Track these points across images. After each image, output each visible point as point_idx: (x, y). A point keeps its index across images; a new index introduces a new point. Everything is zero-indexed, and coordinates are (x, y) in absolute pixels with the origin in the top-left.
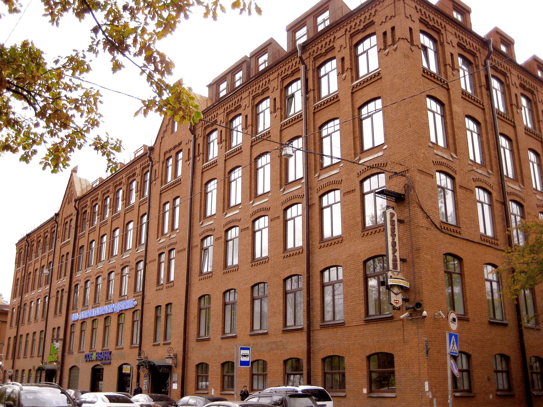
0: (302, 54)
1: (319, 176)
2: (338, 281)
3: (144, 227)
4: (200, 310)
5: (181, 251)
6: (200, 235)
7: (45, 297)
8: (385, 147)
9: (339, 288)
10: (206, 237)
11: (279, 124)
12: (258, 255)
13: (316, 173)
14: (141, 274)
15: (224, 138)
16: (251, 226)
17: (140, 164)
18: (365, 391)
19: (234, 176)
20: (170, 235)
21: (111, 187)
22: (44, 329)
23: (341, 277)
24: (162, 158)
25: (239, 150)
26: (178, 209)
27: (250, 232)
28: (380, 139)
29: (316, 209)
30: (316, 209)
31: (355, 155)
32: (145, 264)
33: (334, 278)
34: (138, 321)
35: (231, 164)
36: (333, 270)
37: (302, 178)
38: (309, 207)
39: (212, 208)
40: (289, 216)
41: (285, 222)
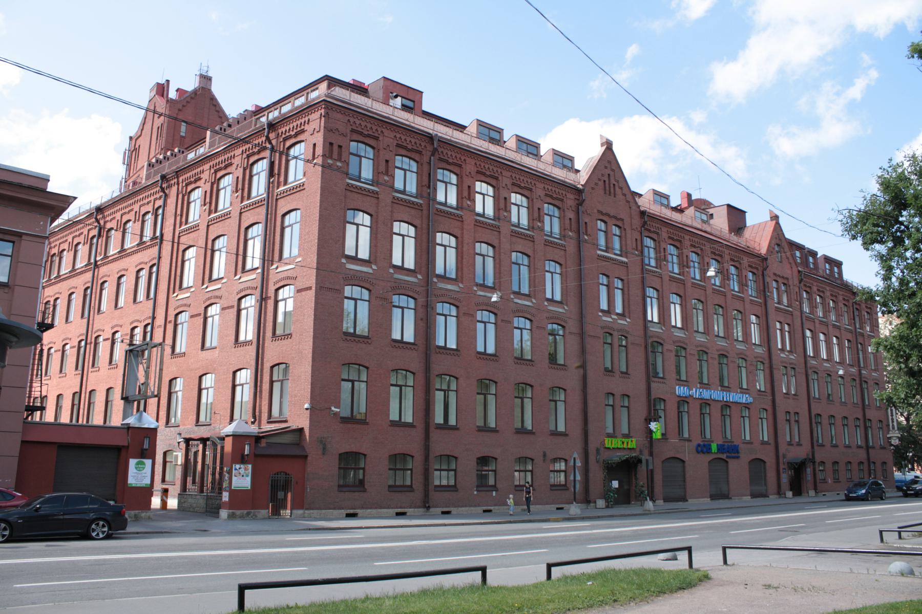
0: (268, 133)
1: (277, 268)
4: (272, 382)
5: (228, 308)
6: (275, 283)
7: (146, 326)
9: (211, 390)
10: (211, 305)
11: (238, 206)
13: (174, 292)
14: (82, 350)
16: (203, 312)
17: (241, 149)
19: (219, 244)
20: (277, 268)
21: (207, 173)
22: (78, 390)
25: (227, 216)
29: (271, 303)
30: (271, 303)
32: (86, 344)
35: (214, 231)
37: (257, 268)
38: (263, 299)
40: (280, 297)
41: (205, 319)
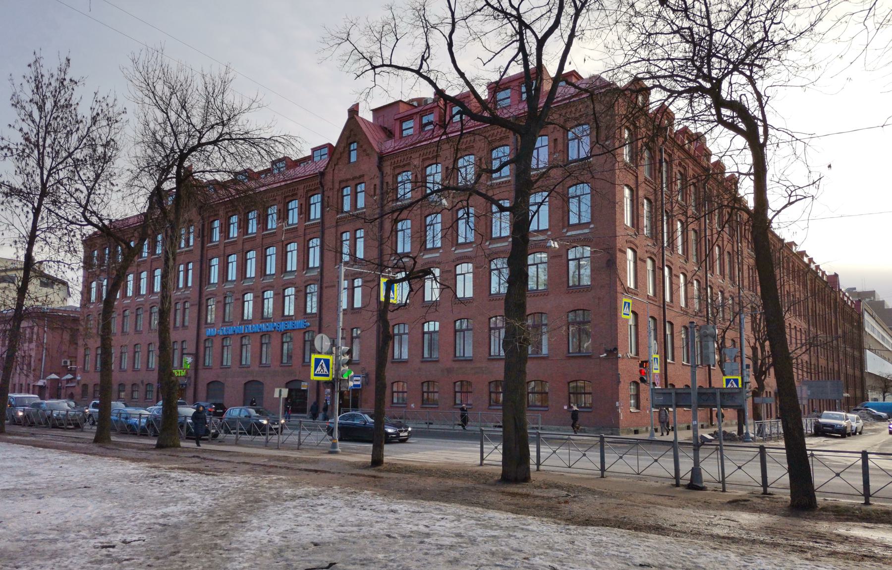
2: (435, 332)
3: (181, 274)
8: (592, 226)
9: (405, 337)
12: (245, 318)
15: (303, 210)
18: (566, 407)
23: (437, 329)
24: (337, 186)
26: (190, 272)
27: (281, 296)
28: (586, 218)
31: (420, 251)
33: (432, 329)
34: (499, 329)
36: (402, 326)
37: (508, 237)
39: (214, 278)
